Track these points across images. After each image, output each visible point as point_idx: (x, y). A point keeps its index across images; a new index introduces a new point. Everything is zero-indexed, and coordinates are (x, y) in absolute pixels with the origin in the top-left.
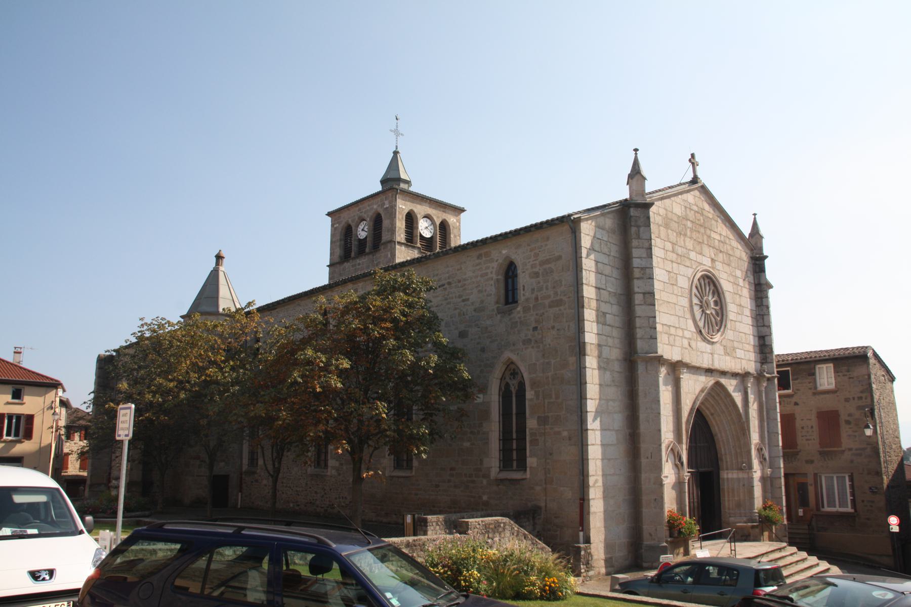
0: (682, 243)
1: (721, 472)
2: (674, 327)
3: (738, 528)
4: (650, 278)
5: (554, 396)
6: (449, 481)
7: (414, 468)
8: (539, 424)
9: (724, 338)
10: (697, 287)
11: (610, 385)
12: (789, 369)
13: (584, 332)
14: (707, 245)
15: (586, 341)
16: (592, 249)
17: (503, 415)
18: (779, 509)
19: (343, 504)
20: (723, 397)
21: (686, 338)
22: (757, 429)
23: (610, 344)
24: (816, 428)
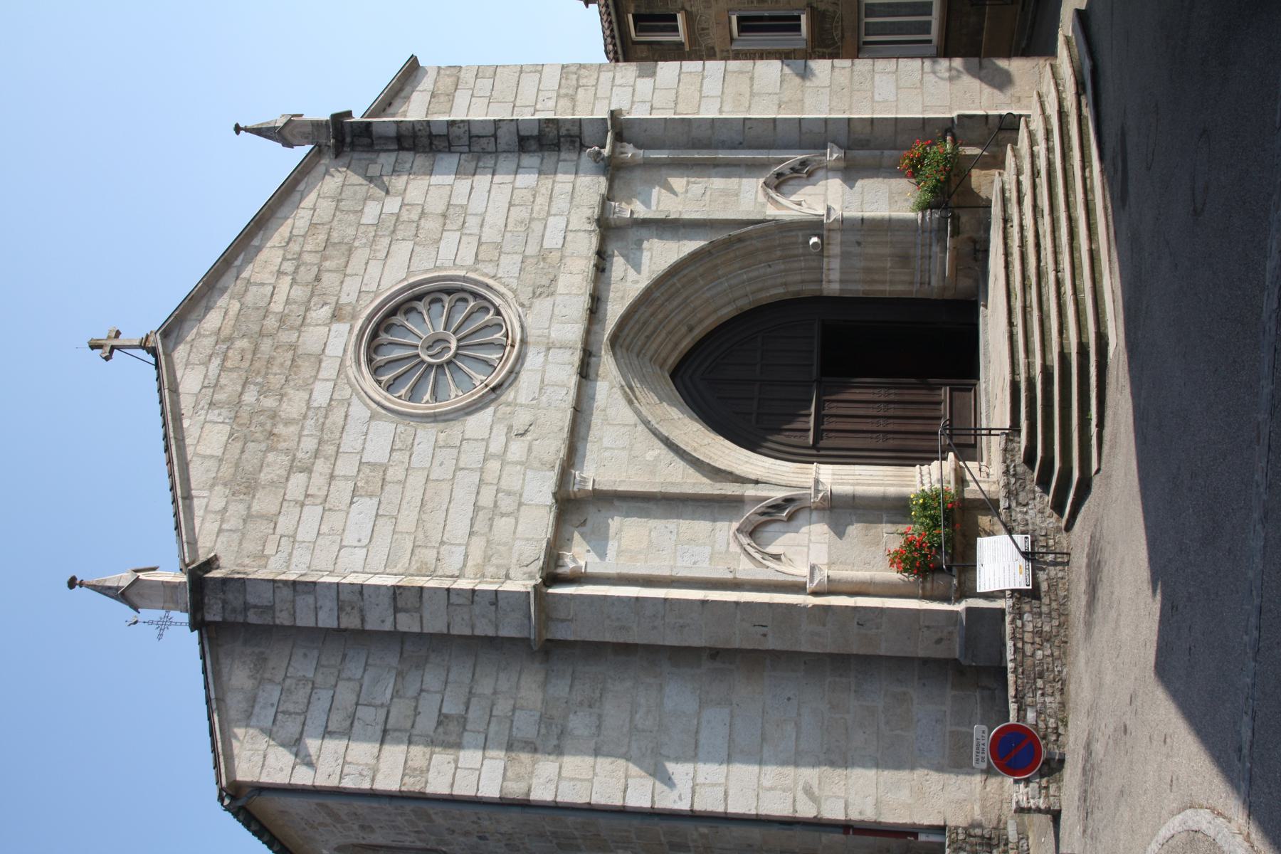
1: (825, 293)
4: (361, 593)
11: (600, 716)
14: (299, 329)
20: (651, 310)
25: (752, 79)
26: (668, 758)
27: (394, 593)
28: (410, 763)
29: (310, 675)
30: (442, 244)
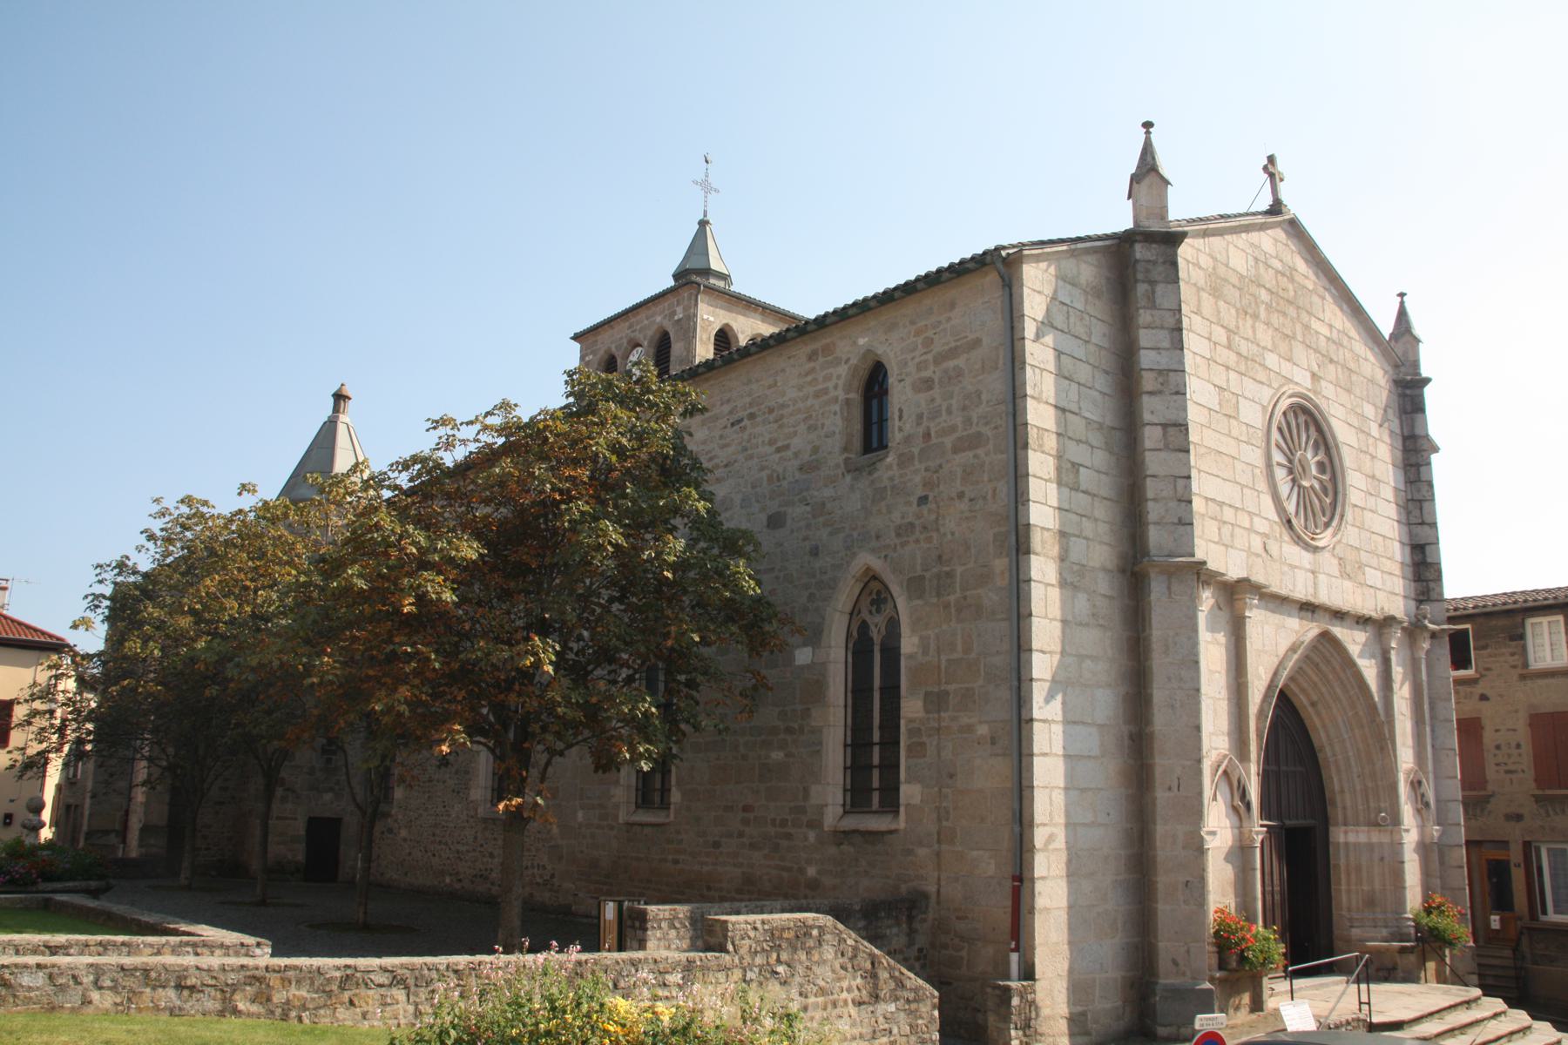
0: (1250, 332)
1: (1332, 829)
2: (1230, 506)
3: (1371, 951)
4: (1177, 393)
5: (959, 648)
6: (741, 835)
7: (672, 807)
8: (927, 711)
9: (1339, 541)
10: (1280, 429)
11: (1087, 625)
12: (1468, 626)
13: (1028, 500)
14: (1303, 342)
15: (1031, 522)
16: (1047, 324)
17: (853, 692)
18: (1459, 912)
19: (539, 880)
20: (1338, 667)
21: (1257, 533)
22: (1410, 741)
23: (1088, 533)
24: (1527, 748)
26: (1065, 695)
27: (1181, 425)
28: (1046, 434)
29: (1094, 340)
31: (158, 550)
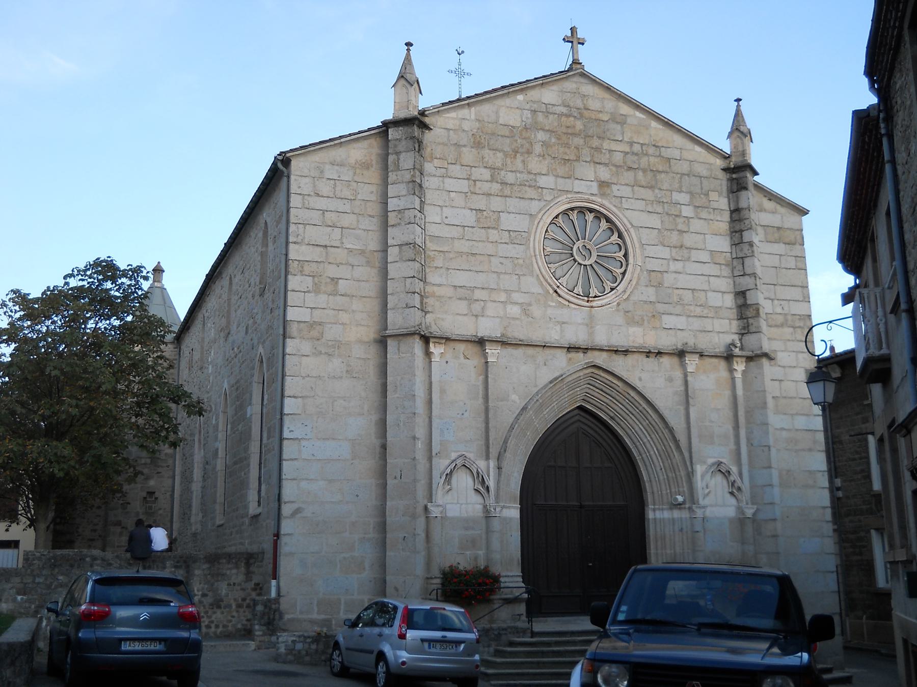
1: (646, 508)
25: (810, 450)
28: (306, 263)
30: (660, 248)
31: (708, 344)
